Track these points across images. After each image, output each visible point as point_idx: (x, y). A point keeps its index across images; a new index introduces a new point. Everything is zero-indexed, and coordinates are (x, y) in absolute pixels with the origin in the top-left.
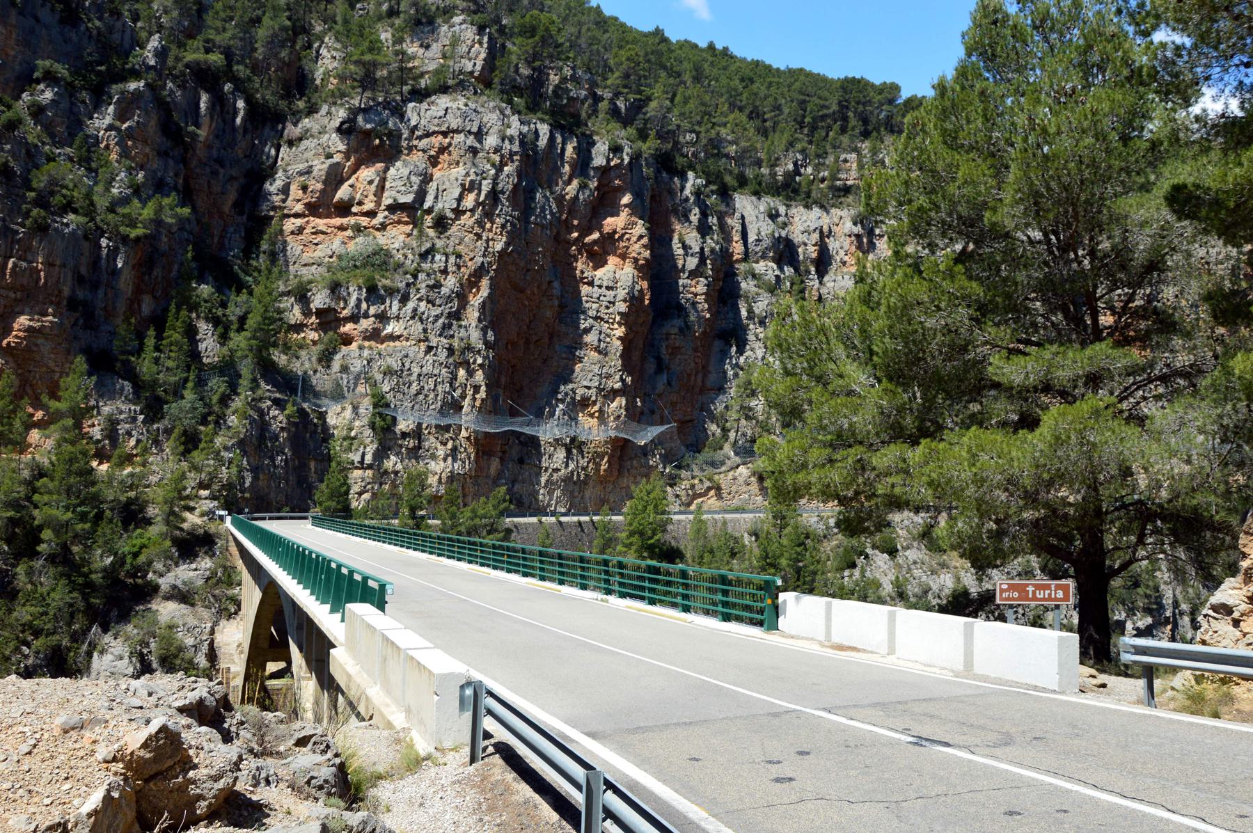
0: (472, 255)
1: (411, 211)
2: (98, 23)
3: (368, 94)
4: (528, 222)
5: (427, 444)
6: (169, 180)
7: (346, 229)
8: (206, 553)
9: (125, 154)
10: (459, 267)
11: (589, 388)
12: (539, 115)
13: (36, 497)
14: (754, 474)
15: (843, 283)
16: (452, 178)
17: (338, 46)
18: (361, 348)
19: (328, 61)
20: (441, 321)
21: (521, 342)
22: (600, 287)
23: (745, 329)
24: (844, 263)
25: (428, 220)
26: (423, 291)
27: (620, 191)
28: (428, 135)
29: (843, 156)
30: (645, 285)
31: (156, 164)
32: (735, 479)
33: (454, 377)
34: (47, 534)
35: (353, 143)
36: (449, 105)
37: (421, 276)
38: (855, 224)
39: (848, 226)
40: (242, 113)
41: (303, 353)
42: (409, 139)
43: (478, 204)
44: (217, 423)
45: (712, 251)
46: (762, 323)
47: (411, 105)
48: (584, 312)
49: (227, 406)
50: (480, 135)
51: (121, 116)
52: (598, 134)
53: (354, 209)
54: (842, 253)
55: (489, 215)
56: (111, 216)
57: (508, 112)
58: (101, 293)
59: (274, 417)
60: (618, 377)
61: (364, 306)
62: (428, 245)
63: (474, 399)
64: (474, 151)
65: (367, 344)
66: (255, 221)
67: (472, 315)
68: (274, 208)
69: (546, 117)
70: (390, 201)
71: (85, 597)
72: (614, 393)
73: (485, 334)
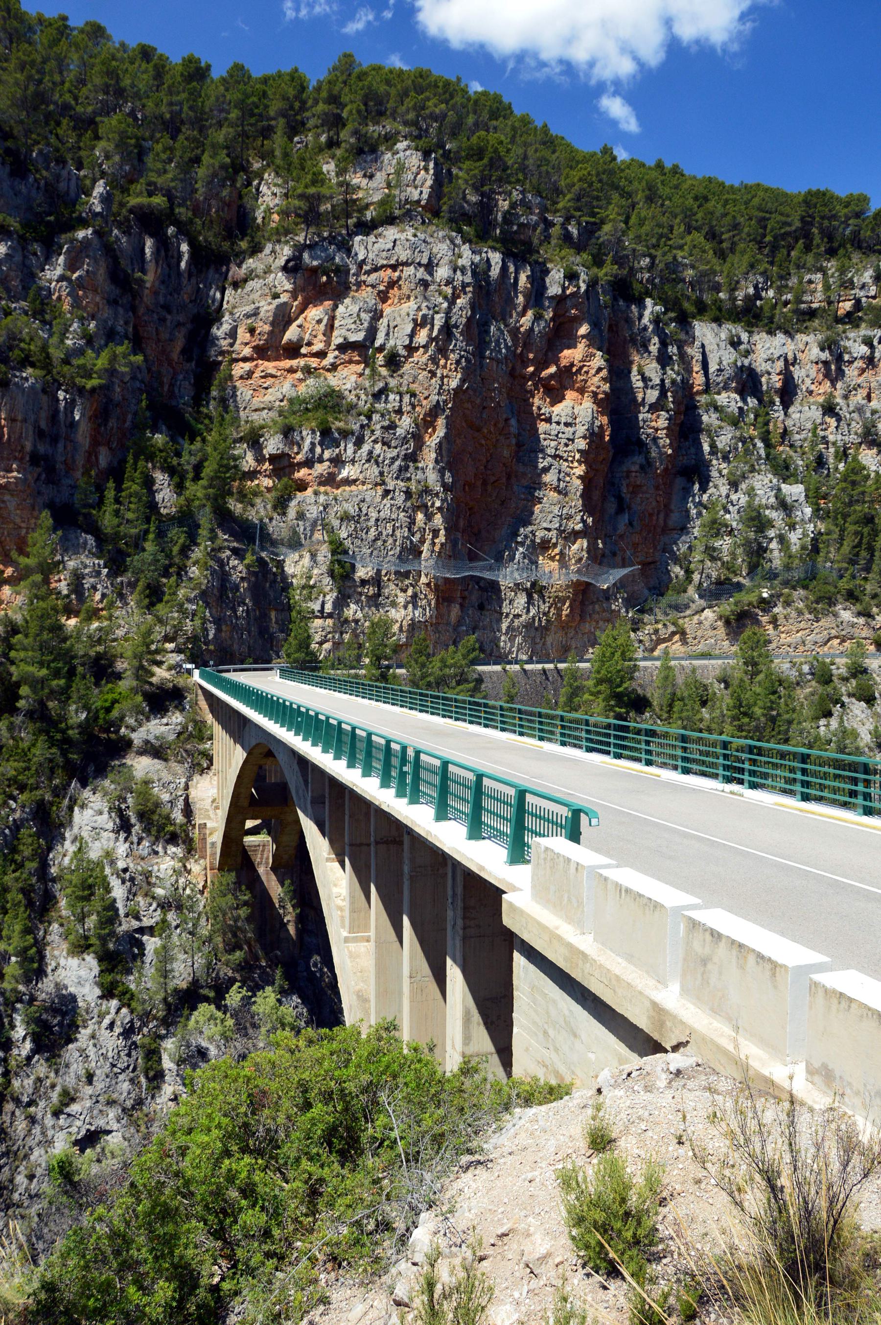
0: (426, 393)
1: (361, 350)
2: (45, 173)
3: (312, 230)
4: (483, 357)
5: (386, 591)
6: (119, 329)
7: (295, 371)
8: (176, 707)
9: (76, 304)
10: (414, 407)
11: (549, 530)
12: (490, 243)
13: (13, 654)
14: (720, 618)
15: (809, 414)
16: (403, 313)
17: (280, 181)
18: (316, 493)
19: (269, 197)
20: (397, 463)
21: (479, 483)
22: (558, 423)
23: (708, 465)
24: (811, 393)
25: (380, 359)
26: (378, 433)
27: (577, 321)
28: (376, 269)
29: (807, 277)
30: (605, 420)
31: (106, 313)
32: (700, 623)
33: (413, 522)
34: (24, 690)
35: (300, 282)
36: (397, 236)
37: (376, 417)
38: (822, 350)
39: (815, 352)
40: (186, 257)
41: (258, 501)
42: (357, 274)
43: (431, 339)
44: (179, 574)
45: (673, 382)
46: (726, 458)
47: (358, 239)
48: (542, 451)
49: (188, 558)
50: (430, 267)
51: (72, 266)
52: (551, 261)
53: (304, 350)
54: (808, 382)
55: (443, 351)
56: (66, 368)
57: (458, 241)
58: (60, 446)
59: (234, 567)
60: (578, 518)
61: (318, 450)
62: (381, 384)
63: (434, 544)
64: (425, 284)
65: (322, 489)
66: (203, 367)
67: (429, 456)
68: (222, 353)
69: (498, 245)
70: (340, 340)
71: (64, 753)
72: (575, 535)
73: (443, 476)
